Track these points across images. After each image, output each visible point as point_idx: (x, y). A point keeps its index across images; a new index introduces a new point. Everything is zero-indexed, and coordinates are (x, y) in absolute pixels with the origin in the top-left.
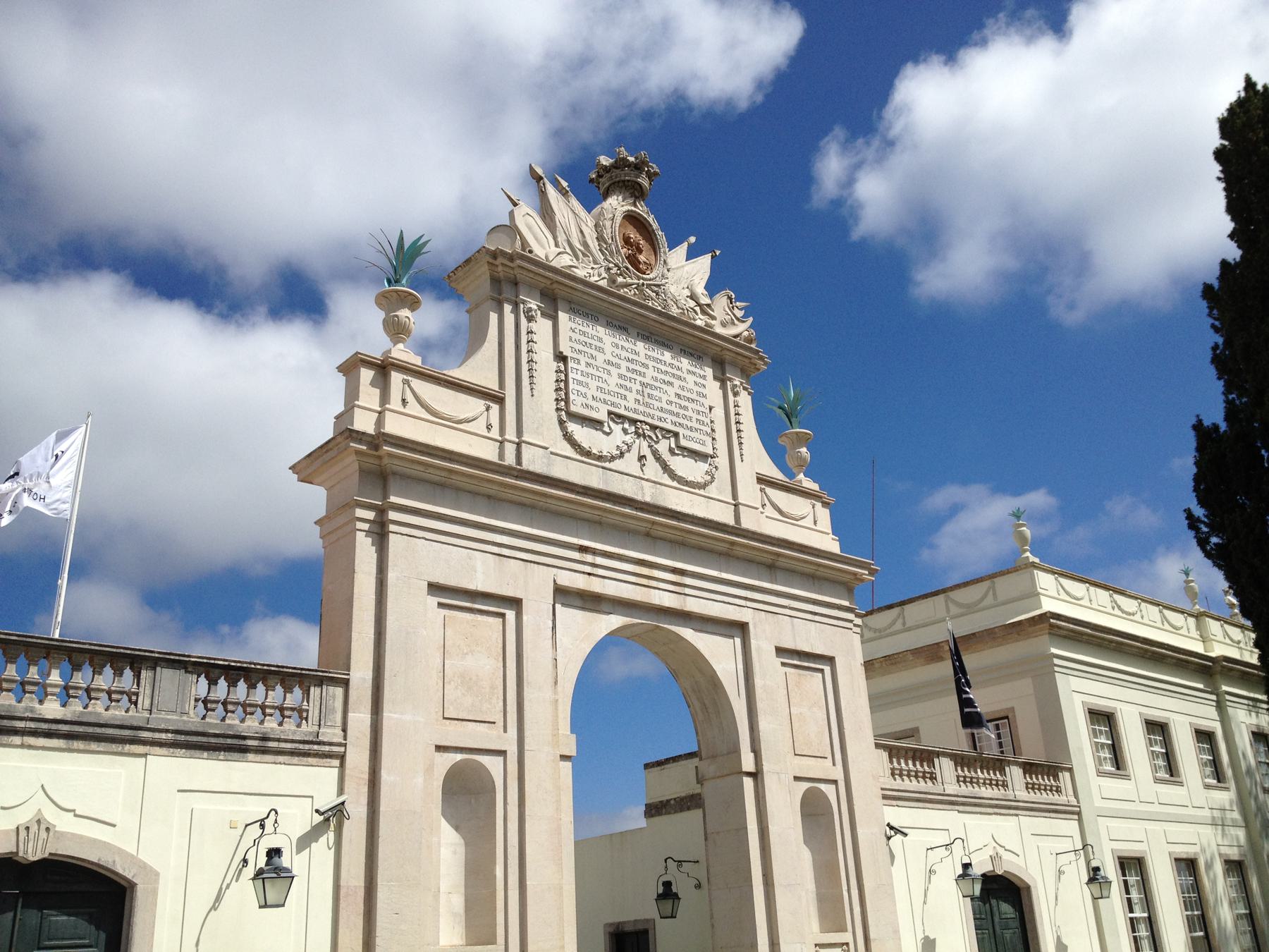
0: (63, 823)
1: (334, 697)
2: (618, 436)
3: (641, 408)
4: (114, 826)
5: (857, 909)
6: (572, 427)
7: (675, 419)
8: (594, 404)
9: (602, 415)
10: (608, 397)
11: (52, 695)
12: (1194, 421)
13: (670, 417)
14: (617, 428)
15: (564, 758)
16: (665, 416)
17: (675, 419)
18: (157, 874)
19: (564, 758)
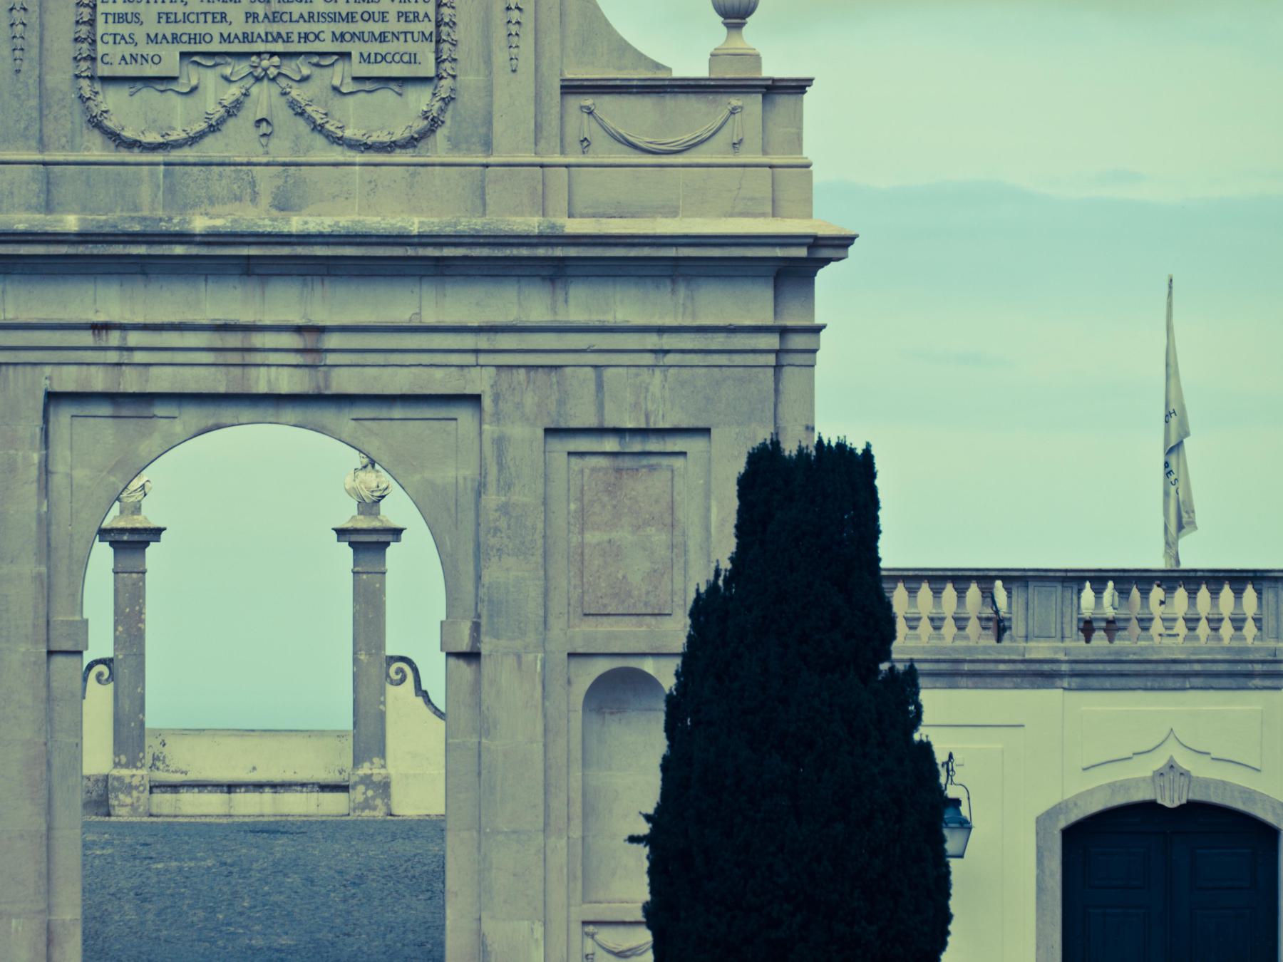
0: (1201, 769)
1: (258, 378)
2: (214, 90)
3: (260, 29)
4: (1085, 769)
5: (399, 381)
6: (113, 101)
7: (340, 27)
8: (150, 50)
9: (169, 61)
10: (179, 29)
11: (1100, 629)
12: (334, 535)
13: (327, 28)
14: (208, 79)
15: (633, 839)
16: (315, 27)
17: (340, 27)
18: (1038, 820)
19: (633, 839)
